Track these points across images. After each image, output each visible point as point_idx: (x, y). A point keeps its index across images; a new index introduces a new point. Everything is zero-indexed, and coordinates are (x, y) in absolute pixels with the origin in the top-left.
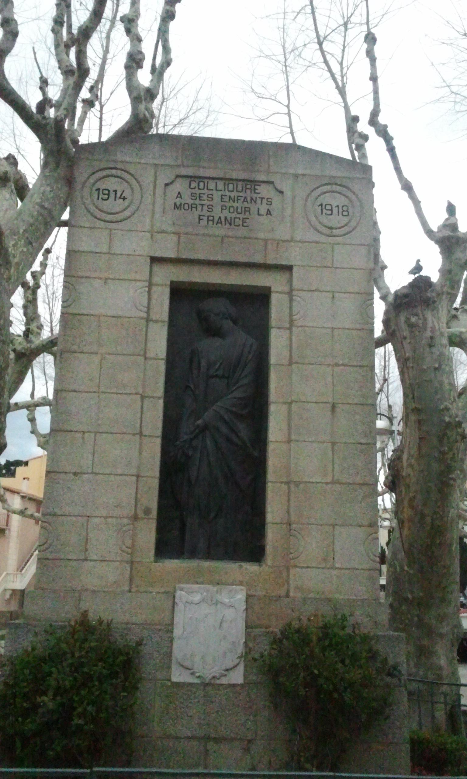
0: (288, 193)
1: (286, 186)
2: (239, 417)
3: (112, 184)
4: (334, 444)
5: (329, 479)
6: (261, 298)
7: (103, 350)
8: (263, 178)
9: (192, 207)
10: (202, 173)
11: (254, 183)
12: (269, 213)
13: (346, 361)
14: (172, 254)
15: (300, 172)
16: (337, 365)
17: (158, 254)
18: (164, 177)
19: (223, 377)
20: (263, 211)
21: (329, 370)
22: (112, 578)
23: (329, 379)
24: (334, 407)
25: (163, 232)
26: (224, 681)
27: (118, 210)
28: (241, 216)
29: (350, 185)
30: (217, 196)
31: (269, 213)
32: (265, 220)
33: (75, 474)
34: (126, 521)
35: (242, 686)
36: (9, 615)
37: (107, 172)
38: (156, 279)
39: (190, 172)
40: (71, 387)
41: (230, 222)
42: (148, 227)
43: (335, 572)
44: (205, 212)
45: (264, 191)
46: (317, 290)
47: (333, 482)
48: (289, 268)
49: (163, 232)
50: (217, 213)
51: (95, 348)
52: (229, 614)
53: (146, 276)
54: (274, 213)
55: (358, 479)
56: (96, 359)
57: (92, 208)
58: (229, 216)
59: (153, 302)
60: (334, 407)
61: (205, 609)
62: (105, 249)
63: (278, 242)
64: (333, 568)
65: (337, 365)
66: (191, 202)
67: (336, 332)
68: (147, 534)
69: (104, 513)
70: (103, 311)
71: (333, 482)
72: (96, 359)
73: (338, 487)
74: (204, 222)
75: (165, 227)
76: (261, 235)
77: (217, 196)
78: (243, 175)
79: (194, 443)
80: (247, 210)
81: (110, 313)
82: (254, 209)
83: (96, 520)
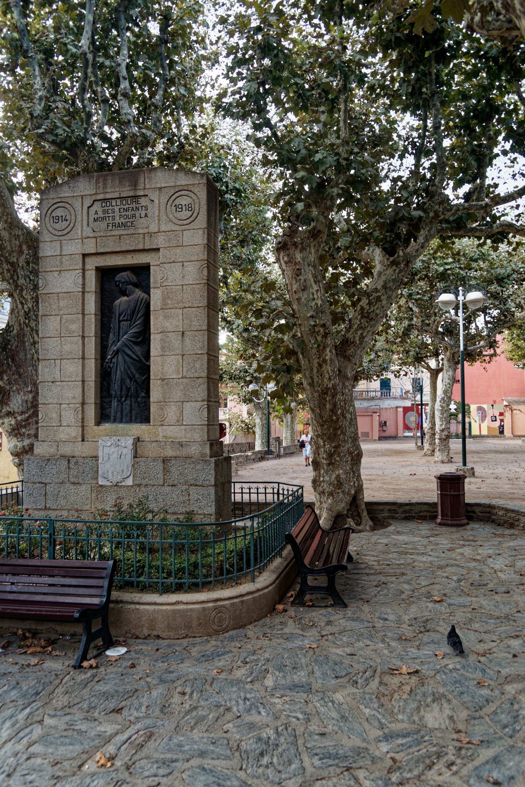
0: (156, 201)
1: (154, 196)
2: (136, 343)
3: (59, 212)
4: (183, 355)
5: (180, 376)
6: (142, 272)
7: (62, 312)
8: (141, 193)
9: (103, 219)
10: (108, 196)
11: (136, 198)
12: (146, 215)
13: (190, 305)
14: (93, 251)
15: (163, 185)
16: (185, 307)
17: (86, 252)
18: (88, 202)
19: (127, 321)
20: (143, 215)
21: (180, 311)
22: (73, 434)
23: (181, 317)
24: (183, 333)
25: (89, 237)
26: (123, 484)
27: (63, 228)
28: (131, 220)
29: (193, 189)
30: (117, 209)
31: (146, 215)
32: (143, 220)
33: (53, 382)
34: (78, 405)
35: (132, 486)
36: (247, 445)
37: (56, 206)
38: (88, 267)
39: (101, 197)
40: (47, 335)
41: (124, 225)
42: (80, 237)
43: (183, 427)
44: (111, 221)
45: (143, 201)
46: (174, 262)
47: (182, 378)
48: (158, 250)
49: (89, 237)
50: (117, 220)
51: (57, 312)
52: (125, 451)
53: (80, 266)
54: (149, 215)
55: (196, 375)
56: (58, 318)
57: (50, 228)
58: (123, 221)
59: (87, 280)
60: (183, 333)
61: (113, 449)
62: (59, 253)
63: (151, 234)
64: (182, 425)
65: (185, 307)
66: (102, 216)
67: (185, 287)
68: (91, 412)
69: (67, 402)
70: (59, 290)
71: (182, 378)
72: (58, 318)
73: (185, 380)
74: (110, 228)
75: (88, 235)
76: (141, 231)
77: (117, 209)
78: (131, 194)
79: (113, 360)
80: (134, 216)
81: (64, 290)
82: (138, 215)
83: (64, 406)
